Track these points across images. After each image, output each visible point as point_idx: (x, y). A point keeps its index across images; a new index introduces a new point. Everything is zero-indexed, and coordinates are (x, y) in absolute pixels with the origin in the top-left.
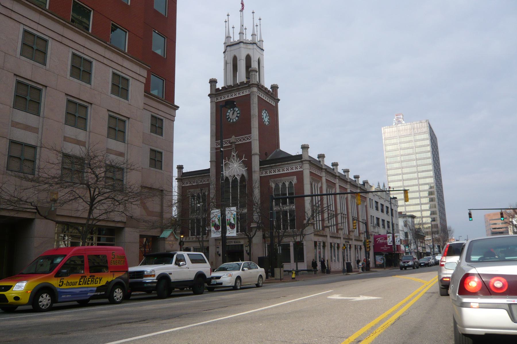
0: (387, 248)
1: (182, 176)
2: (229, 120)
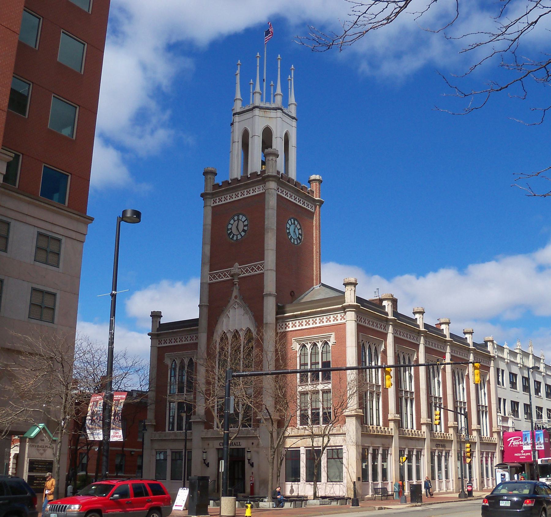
0: (525, 454)
1: (158, 330)
2: (231, 237)
